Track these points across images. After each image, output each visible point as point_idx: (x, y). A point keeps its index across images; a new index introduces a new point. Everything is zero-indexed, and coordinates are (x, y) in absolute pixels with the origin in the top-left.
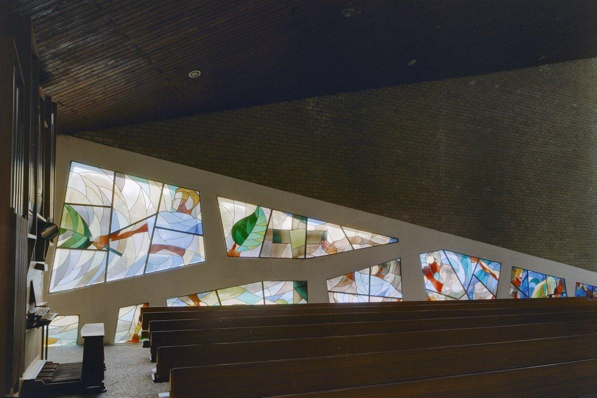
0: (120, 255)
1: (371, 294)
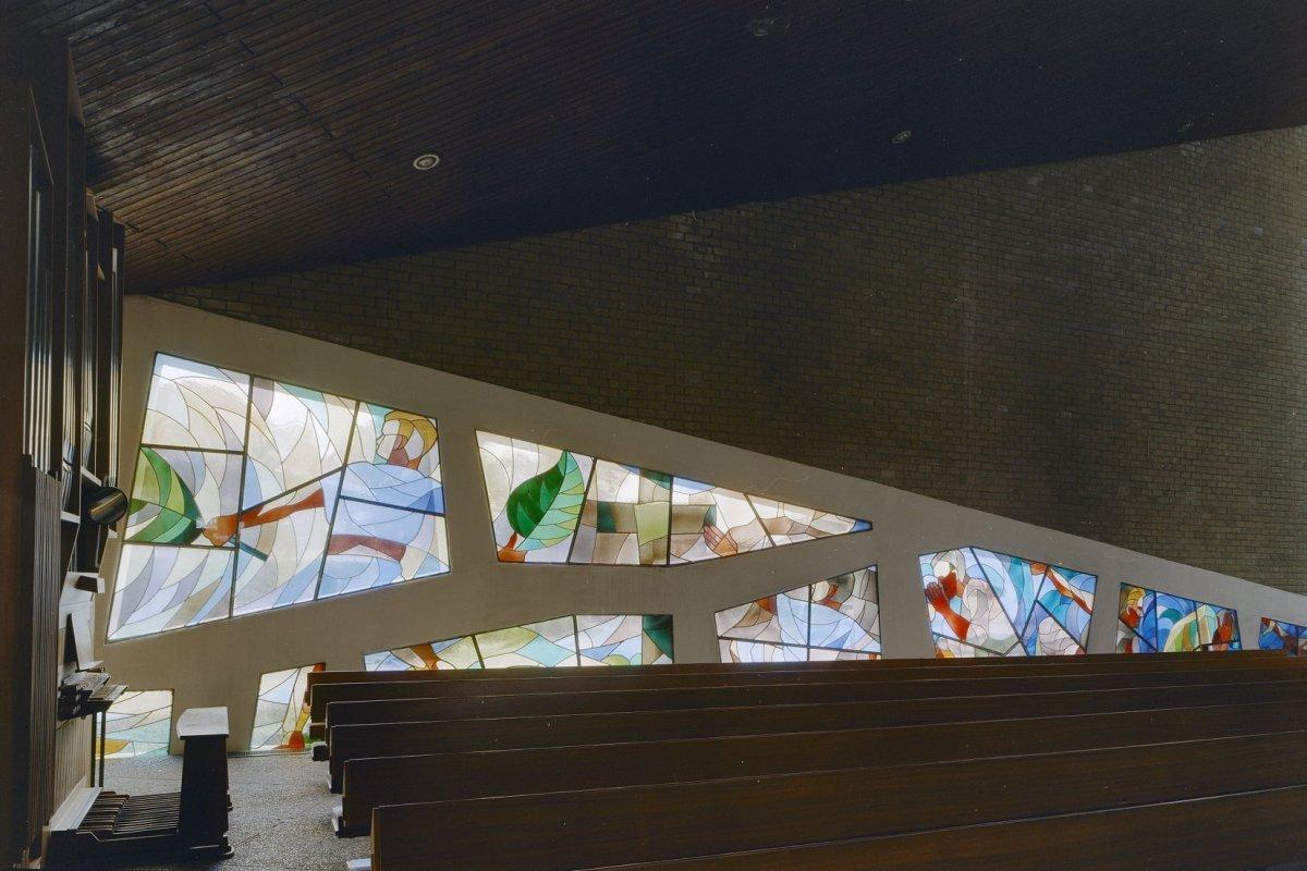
0: (264, 557)
1: (811, 644)
